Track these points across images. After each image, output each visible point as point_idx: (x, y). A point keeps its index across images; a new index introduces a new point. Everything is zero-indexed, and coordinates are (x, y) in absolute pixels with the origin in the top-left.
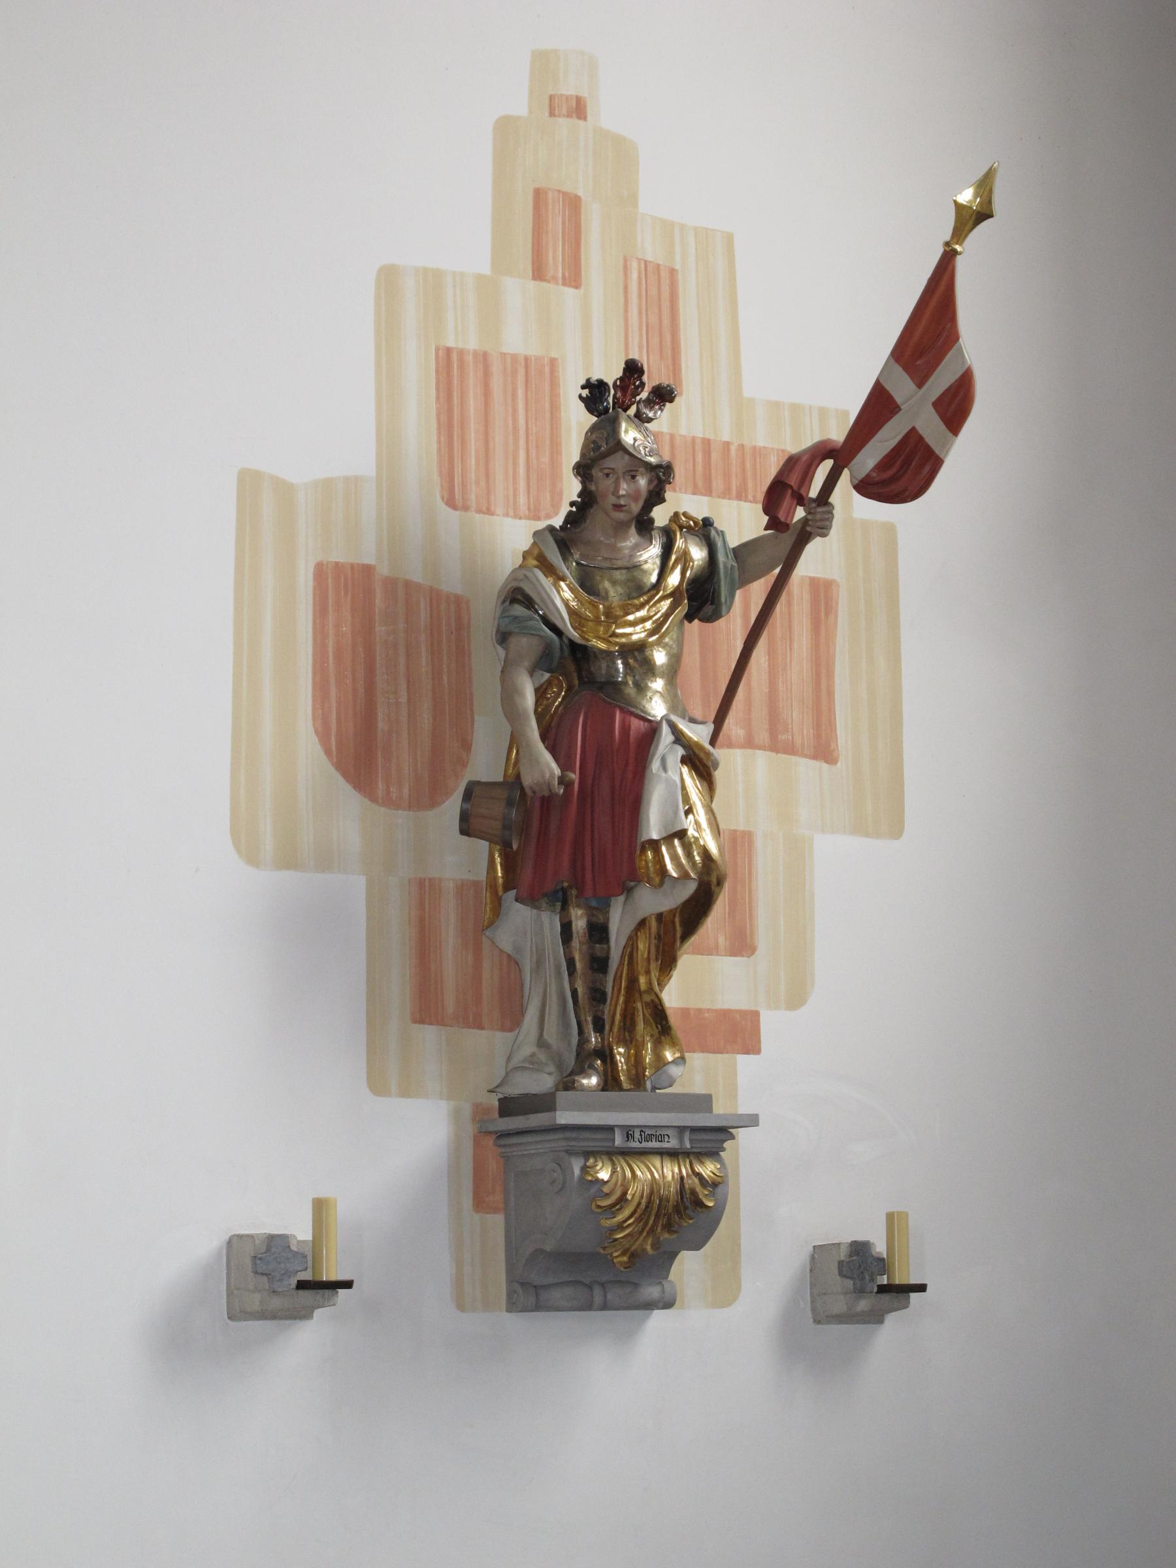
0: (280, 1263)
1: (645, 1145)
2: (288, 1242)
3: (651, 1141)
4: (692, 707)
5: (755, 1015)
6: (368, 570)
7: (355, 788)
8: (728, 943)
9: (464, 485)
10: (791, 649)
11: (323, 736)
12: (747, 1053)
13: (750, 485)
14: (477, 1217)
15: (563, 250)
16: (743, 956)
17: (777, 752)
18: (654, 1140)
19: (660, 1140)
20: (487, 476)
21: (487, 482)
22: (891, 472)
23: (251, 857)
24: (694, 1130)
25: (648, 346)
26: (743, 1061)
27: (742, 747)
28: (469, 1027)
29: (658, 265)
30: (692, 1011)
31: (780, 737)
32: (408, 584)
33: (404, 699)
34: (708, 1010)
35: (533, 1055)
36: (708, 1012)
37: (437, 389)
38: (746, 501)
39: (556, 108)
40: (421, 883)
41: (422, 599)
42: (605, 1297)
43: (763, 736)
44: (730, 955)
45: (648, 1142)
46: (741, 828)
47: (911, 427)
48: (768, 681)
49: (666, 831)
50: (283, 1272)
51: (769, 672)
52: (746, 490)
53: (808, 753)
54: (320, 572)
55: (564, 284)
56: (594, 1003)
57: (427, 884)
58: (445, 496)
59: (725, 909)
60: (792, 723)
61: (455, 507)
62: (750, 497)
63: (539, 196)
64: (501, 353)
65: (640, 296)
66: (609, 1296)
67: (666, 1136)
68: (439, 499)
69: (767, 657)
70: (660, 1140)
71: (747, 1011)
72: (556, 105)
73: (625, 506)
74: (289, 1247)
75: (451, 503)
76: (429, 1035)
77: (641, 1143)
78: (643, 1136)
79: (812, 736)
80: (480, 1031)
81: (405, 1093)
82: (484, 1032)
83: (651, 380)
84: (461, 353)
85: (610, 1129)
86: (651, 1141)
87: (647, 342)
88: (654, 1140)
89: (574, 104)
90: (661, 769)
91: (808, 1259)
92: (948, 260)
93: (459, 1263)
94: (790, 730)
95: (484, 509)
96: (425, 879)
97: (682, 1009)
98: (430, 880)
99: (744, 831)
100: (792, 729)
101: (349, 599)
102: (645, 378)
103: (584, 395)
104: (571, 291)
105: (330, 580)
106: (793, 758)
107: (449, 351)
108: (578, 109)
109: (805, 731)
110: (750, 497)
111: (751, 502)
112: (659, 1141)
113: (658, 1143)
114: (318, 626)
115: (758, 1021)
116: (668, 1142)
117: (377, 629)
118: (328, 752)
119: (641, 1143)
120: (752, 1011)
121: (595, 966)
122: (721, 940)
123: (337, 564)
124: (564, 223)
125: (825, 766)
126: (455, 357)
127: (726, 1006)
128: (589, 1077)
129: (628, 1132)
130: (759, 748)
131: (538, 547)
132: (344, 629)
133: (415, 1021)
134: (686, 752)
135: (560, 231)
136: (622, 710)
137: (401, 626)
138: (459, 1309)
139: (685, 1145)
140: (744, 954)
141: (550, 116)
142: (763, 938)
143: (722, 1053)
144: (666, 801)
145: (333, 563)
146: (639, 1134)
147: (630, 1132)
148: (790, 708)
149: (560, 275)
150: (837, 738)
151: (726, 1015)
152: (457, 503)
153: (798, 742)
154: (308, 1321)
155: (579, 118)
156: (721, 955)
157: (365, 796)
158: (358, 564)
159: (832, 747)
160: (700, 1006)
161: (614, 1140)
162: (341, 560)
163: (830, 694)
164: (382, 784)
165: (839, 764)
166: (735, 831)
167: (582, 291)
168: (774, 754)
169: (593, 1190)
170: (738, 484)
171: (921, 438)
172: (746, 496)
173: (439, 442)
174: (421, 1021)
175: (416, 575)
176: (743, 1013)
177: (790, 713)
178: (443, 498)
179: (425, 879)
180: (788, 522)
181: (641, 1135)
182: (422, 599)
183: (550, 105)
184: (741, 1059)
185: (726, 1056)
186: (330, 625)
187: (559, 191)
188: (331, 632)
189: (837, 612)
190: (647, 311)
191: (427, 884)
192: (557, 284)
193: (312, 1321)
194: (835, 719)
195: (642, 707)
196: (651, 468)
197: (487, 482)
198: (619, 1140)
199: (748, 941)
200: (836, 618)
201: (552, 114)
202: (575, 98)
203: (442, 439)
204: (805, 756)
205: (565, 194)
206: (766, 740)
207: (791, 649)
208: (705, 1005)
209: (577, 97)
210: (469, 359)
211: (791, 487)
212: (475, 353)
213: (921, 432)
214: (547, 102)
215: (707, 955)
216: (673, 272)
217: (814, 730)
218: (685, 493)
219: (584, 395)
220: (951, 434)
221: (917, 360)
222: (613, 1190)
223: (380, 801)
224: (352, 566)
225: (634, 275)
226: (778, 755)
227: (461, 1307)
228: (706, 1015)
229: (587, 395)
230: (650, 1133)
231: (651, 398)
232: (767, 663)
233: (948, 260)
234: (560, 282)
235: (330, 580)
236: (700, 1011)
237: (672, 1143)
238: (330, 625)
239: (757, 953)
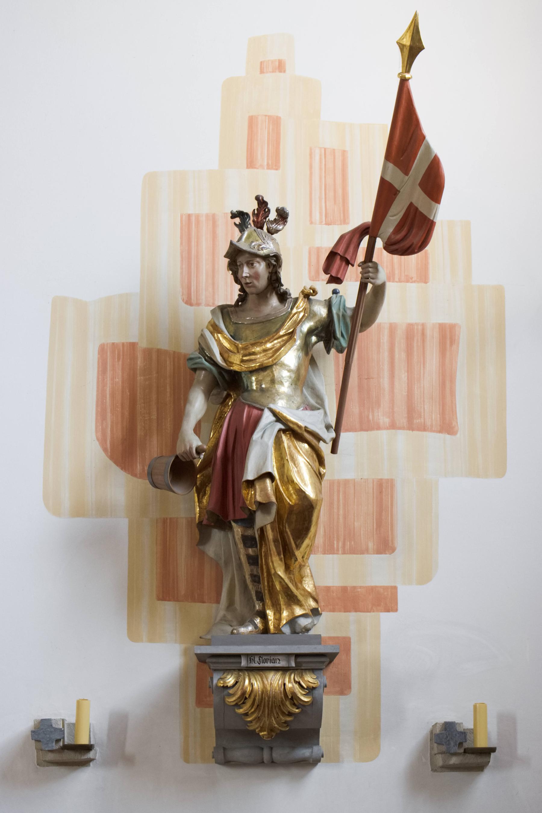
0: (46, 734)
1: (262, 665)
2: (51, 723)
3: (267, 663)
4: (352, 408)
5: (395, 588)
6: (133, 346)
7: (122, 469)
8: (375, 547)
9: (197, 291)
10: (424, 367)
11: (102, 442)
12: (388, 611)
13: (397, 272)
14: (198, 710)
15: (268, 150)
16: (386, 554)
17: (413, 430)
18: (269, 662)
19: (273, 662)
20: (213, 284)
21: (213, 288)
22: (403, 233)
23: (56, 511)
24: (297, 656)
25: (325, 198)
26: (385, 617)
27: (387, 429)
28: (195, 602)
29: (334, 150)
30: (349, 588)
31: (415, 421)
32: (159, 351)
33: (154, 417)
34: (361, 587)
35: (224, 616)
36: (360, 588)
37: (181, 238)
38: (393, 282)
39: (265, 69)
40: (164, 521)
41: (168, 359)
42: (271, 755)
43: (402, 420)
44: (377, 554)
45: (264, 663)
46: (386, 477)
47: (410, 202)
48: (406, 388)
49: (257, 473)
50: (48, 739)
51: (408, 384)
52: (394, 275)
53: (436, 430)
54: (102, 349)
55: (268, 168)
56: (255, 584)
57: (168, 521)
58: (185, 299)
59: (373, 526)
60: (424, 413)
61: (191, 305)
62: (397, 279)
63: (252, 121)
64: (224, 213)
65: (321, 169)
66: (274, 755)
67: (277, 660)
68: (181, 301)
69: (406, 374)
70: (273, 662)
71: (389, 586)
72: (265, 67)
73: (251, 283)
74: (52, 725)
75: (189, 302)
76: (169, 607)
77: (259, 664)
78: (261, 660)
79: (439, 419)
80: (203, 604)
81: (151, 640)
82: (205, 604)
83: (273, 206)
84: (198, 216)
85: (239, 656)
86: (267, 663)
87: (325, 195)
88: (269, 662)
89: (277, 64)
90: (260, 437)
91: (429, 734)
92: (404, 82)
93: (186, 737)
94: (422, 417)
95: (211, 304)
96: (167, 519)
97: (342, 587)
98: (170, 519)
99: (388, 480)
100: (424, 415)
101: (120, 363)
102: (269, 206)
103: (238, 223)
104: (273, 172)
105: (109, 353)
106: (425, 433)
107: (189, 216)
108: (280, 67)
109: (434, 416)
110: (397, 279)
111: (397, 282)
112: (272, 662)
113: (272, 664)
114: (100, 380)
115: (396, 593)
116: (279, 663)
117: (139, 378)
118: (105, 450)
119: (259, 664)
120: (391, 587)
121: (251, 561)
122: (371, 545)
123: (113, 344)
124: (269, 133)
125: (448, 436)
126: (193, 219)
127: (373, 584)
128: (246, 626)
129: (250, 656)
130: (400, 428)
131: (213, 319)
132: (117, 380)
133: (159, 599)
134: (285, 427)
135: (266, 138)
136: (249, 406)
137: (155, 375)
138: (185, 762)
139: (291, 664)
140: (387, 552)
141: (261, 73)
142: (400, 542)
143: (370, 612)
144: (260, 457)
145: (111, 344)
146: (259, 658)
147: (252, 658)
148: (422, 403)
149: (266, 163)
150: (457, 418)
151: (372, 589)
152: (192, 301)
153: (428, 423)
154: (87, 767)
155: (280, 72)
156: (370, 554)
157: (129, 474)
158: (127, 343)
159: (453, 425)
160: (354, 584)
161: (241, 663)
162: (116, 341)
163: (453, 393)
164: (140, 466)
165: (458, 435)
166: (381, 479)
167: (279, 171)
168: (411, 432)
169: (225, 692)
170: (388, 272)
171: (416, 209)
172: (394, 279)
173: (182, 268)
174: (163, 599)
175: (164, 345)
176: (385, 588)
177: (422, 406)
178: (183, 300)
179: (167, 519)
180: (339, 276)
181: (260, 659)
182: (168, 359)
183: (261, 67)
184: (384, 616)
185: (372, 614)
186: (108, 379)
187: (266, 116)
188: (108, 382)
189: (458, 343)
190: (325, 177)
191: (168, 521)
192: (264, 169)
193: (90, 767)
194: (456, 408)
195: (261, 403)
196: (266, 258)
197: (213, 288)
198: (244, 663)
199: (390, 544)
200: (458, 346)
201: (262, 72)
202: (278, 61)
203: (184, 266)
204: (434, 431)
205: (269, 117)
206: (405, 424)
207: (424, 367)
208: (359, 583)
209: (279, 60)
210: (203, 219)
211: (339, 254)
212: (207, 215)
213: (416, 205)
214: (259, 67)
215: (360, 554)
216: (344, 153)
217: (440, 415)
218: (350, 281)
219: (238, 223)
220: (433, 203)
221: (401, 158)
222: (236, 692)
223: (138, 475)
224: (123, 344)
225: (317, 158)
226: (413, 432)
227: (187, 760)
228: (359, 590)
229: (239, 223)
230: (266, 658)
231: (277, 218)
232: (406, 378)
233: (404, 82)
234: (265, 168)
235: (109, 353)
236: (354, 588)
237: (283, 663)
238: (108, 379)
239: (396, 551)
